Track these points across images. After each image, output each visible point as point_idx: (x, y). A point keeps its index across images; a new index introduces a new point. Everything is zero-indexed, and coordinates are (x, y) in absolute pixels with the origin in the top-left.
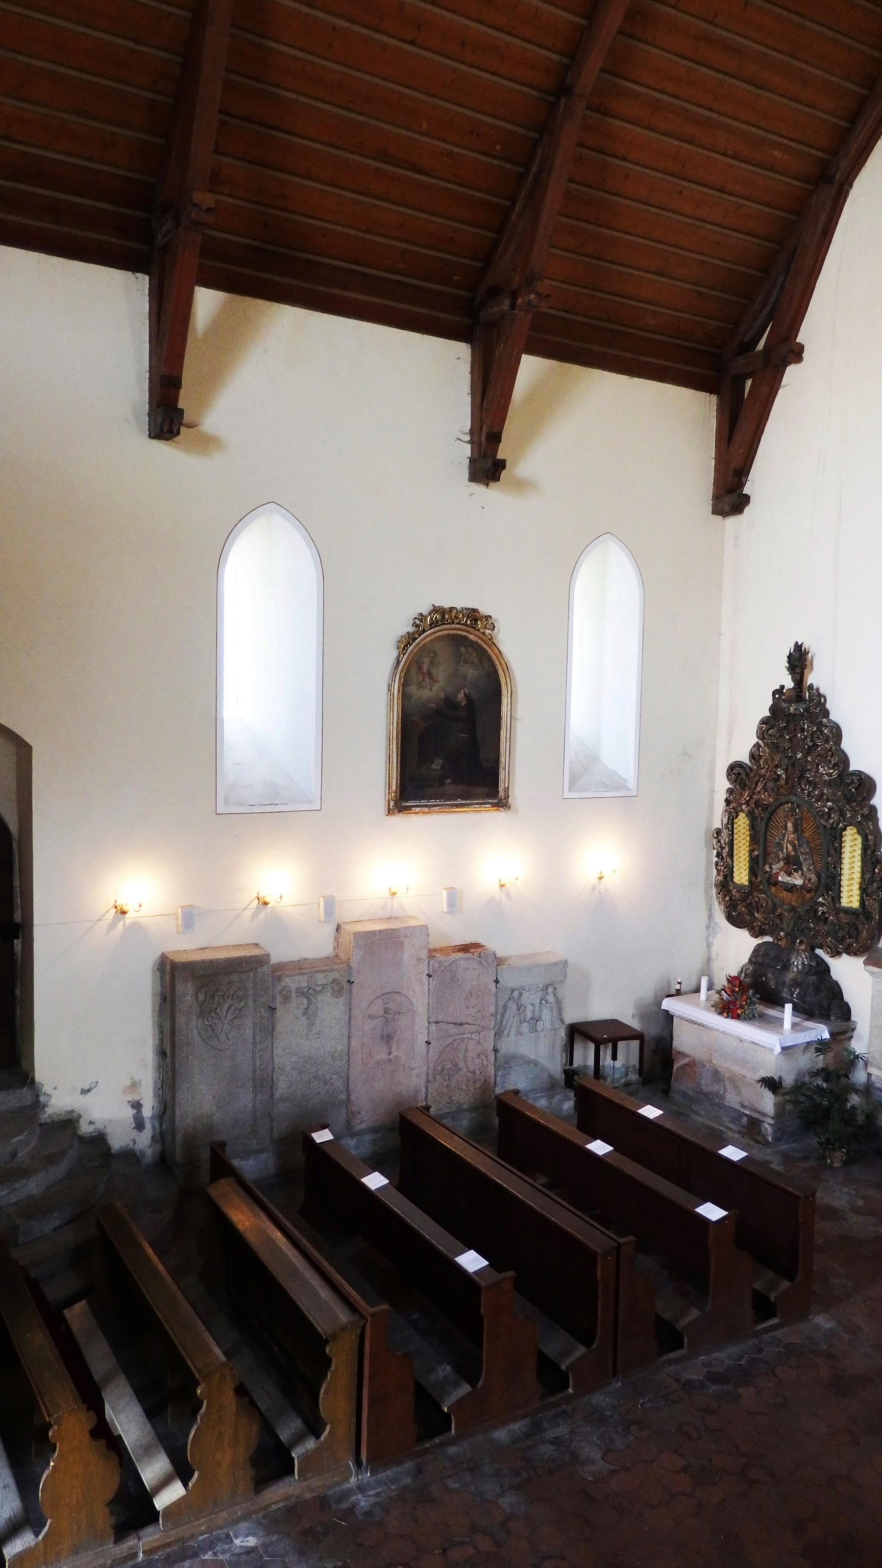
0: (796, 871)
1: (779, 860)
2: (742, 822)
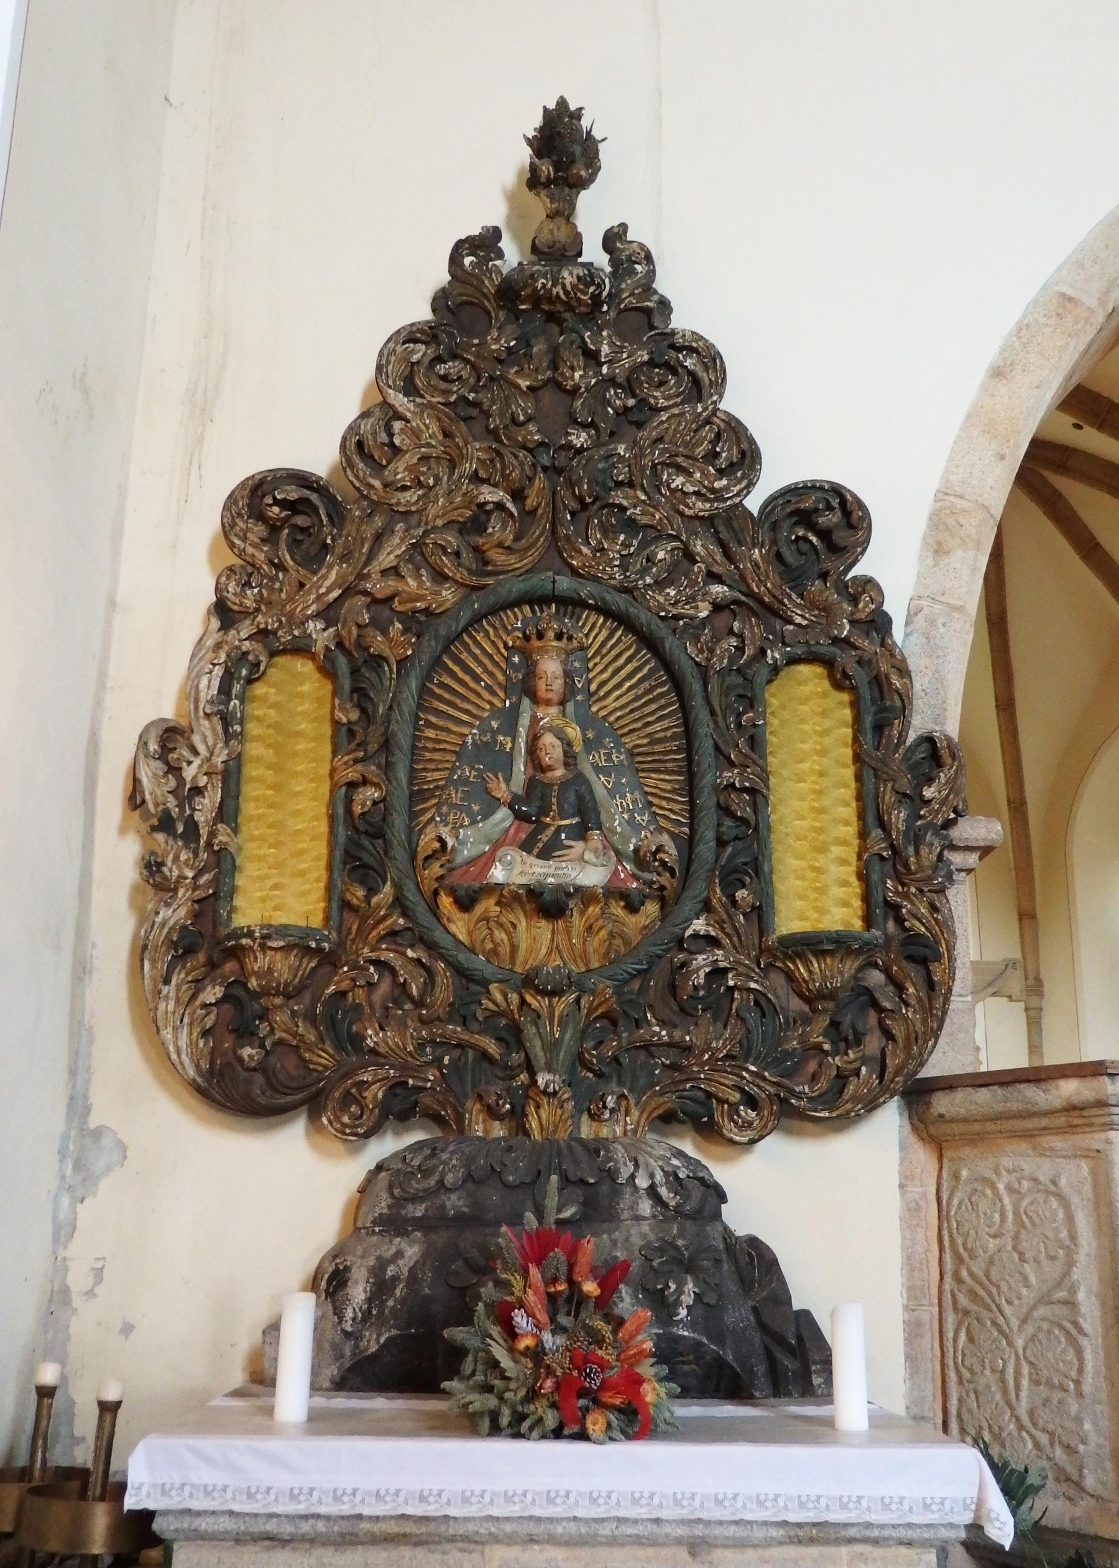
0: (581, 833)
1: (491, 804)
2: (297, 702)
